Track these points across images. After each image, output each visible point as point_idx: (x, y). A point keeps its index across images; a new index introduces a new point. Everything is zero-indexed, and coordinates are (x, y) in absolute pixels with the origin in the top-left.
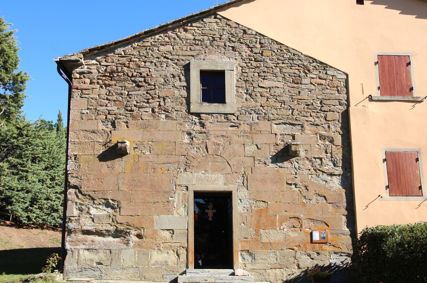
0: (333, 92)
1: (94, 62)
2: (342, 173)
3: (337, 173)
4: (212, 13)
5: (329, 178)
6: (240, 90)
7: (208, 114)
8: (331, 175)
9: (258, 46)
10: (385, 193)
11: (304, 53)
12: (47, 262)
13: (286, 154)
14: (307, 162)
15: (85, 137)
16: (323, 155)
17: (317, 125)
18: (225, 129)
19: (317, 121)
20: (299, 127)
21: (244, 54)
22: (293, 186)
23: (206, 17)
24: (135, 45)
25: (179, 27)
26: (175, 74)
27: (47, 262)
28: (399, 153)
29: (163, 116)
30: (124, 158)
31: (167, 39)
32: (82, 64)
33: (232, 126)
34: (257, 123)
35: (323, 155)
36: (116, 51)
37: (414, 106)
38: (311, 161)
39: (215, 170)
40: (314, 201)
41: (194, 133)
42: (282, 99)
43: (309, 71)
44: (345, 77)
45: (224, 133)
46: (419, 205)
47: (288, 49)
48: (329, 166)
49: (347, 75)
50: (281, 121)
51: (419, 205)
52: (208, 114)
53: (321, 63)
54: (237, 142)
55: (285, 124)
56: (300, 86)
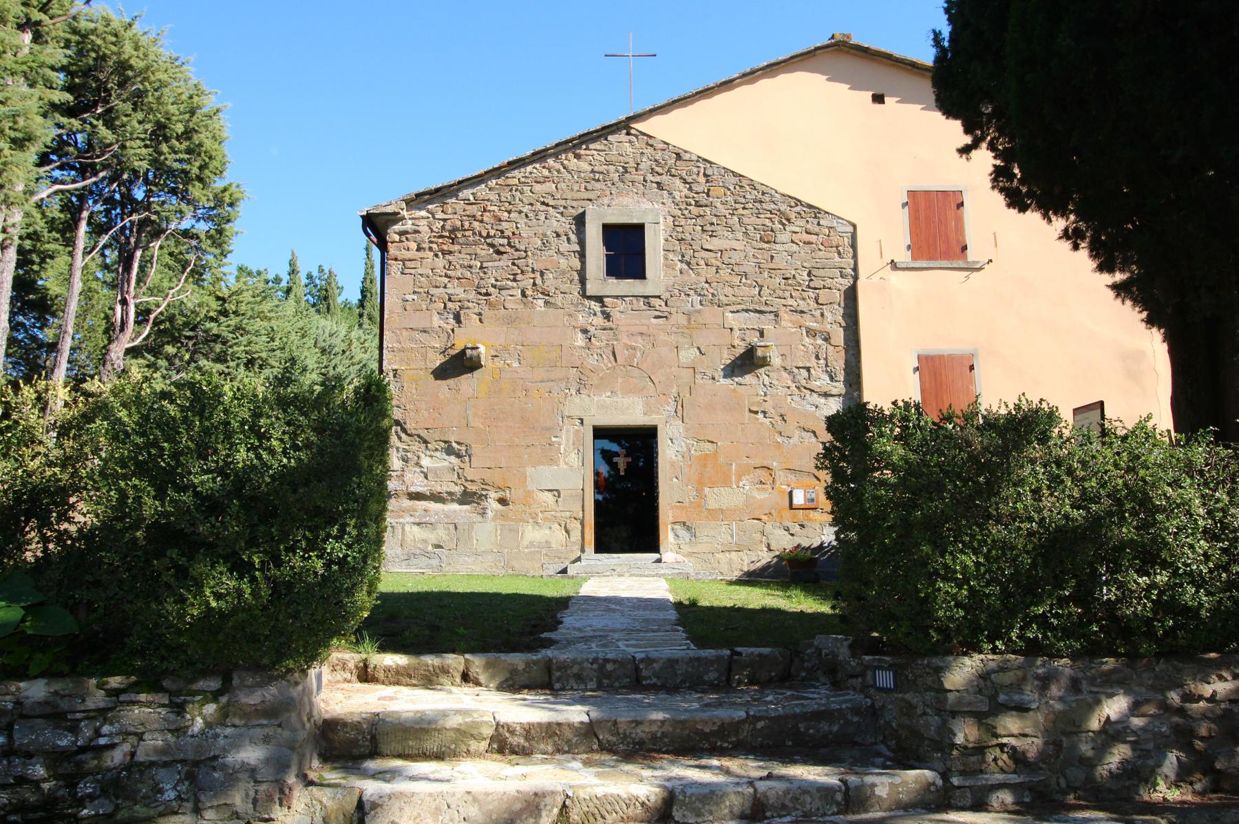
0: (830, 255)
1: (423, 213)
2: (843, 392)
3: (835, 391)
4: (624, 126)
5: (823, 400)
6: (671, 256)
7: (617, 297)
8: (826, 395)
9: (702, 179)
11: (780, 190)
13: (747, 362)
14: (785, 375)
16: (812, 362)
18: (644, 321)
19: (803, 306)
21: (677, 194)
22: (760, 416)
23: (612, 133)
28: (941, 357)
29: (541, 302)
30: (477, 373)
31: (546, 172)
34: (699, 312)
35: (812, 362)
37: (967, 277)
38: (791, 373)
39: (628, 391)
40: (795, 440)
42: (742, 269)
43: (788, 220)
45: (644, 329)
47: (752, 185)
49: (854, 226)
50: (740, 307)
53: (810, 206)
55: (747, 311)
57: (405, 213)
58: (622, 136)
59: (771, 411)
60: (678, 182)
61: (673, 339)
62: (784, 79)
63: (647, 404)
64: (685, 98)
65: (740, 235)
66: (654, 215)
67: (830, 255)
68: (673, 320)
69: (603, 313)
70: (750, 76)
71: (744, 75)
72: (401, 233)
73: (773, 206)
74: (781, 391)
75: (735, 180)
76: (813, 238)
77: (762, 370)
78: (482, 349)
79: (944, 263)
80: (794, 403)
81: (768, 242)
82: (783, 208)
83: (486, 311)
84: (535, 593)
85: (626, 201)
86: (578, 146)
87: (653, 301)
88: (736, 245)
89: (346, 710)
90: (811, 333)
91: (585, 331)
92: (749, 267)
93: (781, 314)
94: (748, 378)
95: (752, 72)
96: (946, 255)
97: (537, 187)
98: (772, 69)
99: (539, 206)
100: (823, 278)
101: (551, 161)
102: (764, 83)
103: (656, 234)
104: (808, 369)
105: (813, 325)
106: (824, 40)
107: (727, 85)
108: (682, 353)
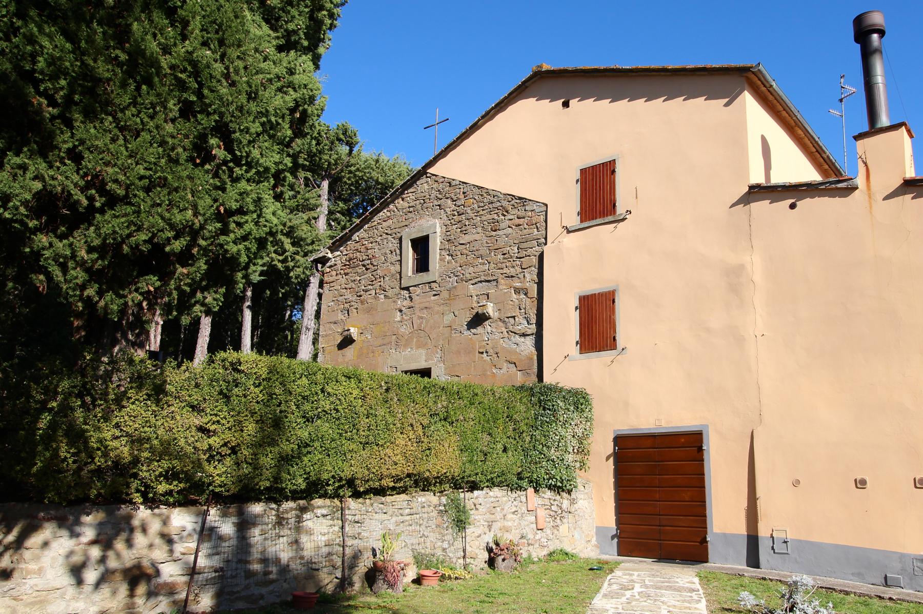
0: (531, 231)
1: (339, 253)
2: (535, 331)
3: (529, 332)
4: (422, 172)
5: (522, 339)
6: (443, 253)
7: (415, 286)
8: (524, 335)
9: (462, 196)
10: (574, 350)
11: (503, 192)
12: (33, 13)
13: (478, 320)
14: (501, 324)
15: (330, 329)
16: (516, 312)
17: (512, 277)
18: (428, 299)
19: (512, 271)
20: (495, 283)
21: (448, 210)
22: (485, 355)
23: (419, 179)
24: (366, 227)
25: (397, 198)
26: (393, 249)
27: (33, 13)
28: (593, 296)
29: (382, 296)
30: (354, 344)
31: (389, 214)
32: (330, 259)
33: (435, 295)
34: (455, 287)
35: (516, 312)
36: (353, 238)
37: (616, 227)
38: (504, 322)
39: (418, 347)
40: (504, 370)
41: (403, 309)
42: (480, 253)
43: (507, 212)
44: (545, 209)
45: (427, 305)
46: (612, 362)
47: (488, 192)
48: (523, 326)
49: (546, 205)
50: (477, 280)
51: (612, 362)
52: (415, 286)
53: (520, 198)
54: (438, 313)
55: (481, 282)
56: (498, 233)
57: (330, 255)
58: (423, 179)
59: (491, 351)
60: (449, 201)
61: (441, 309)
62: (512, 109)
63: (427, 354)
64: (454, 142)
65: (479, 230)
66: (434, 227)
67: (531, 231)
68: (442, 294)
69: (410, 297)
70: (489, 116)
71: (483, 117)
72: (330, 267)
73: (499, 204)
74: (498, 336)
75: (476, 191)
76: (521, 221)
77: (487, 323)
78: (352, 330)
79: (599, 221)
80: (503, 343)
81: (495, 231)
82: (505, 203)
83: (360, 306)
84: (612, 480)
85: (422, 222)
86: (402, 193)
87: (433, 285)
88: (477, 237)
89: (644, 566)
90: (517, 291)
91: (401, 311)
92: (484, 251)
93: (500, 280)
94: (479, 330)
95: (487, 113)
96: (603, 214)
97: (385, 224)
98: (501, 106)
99: (385, 236)
100: (525, 249)
101: (391, 206)
102: (500, 117)
103: (435, 240)
104: (514, 317)
105: (518, 285)
106: (529, 74)
107: (475, 127)
108: (445, 317)
